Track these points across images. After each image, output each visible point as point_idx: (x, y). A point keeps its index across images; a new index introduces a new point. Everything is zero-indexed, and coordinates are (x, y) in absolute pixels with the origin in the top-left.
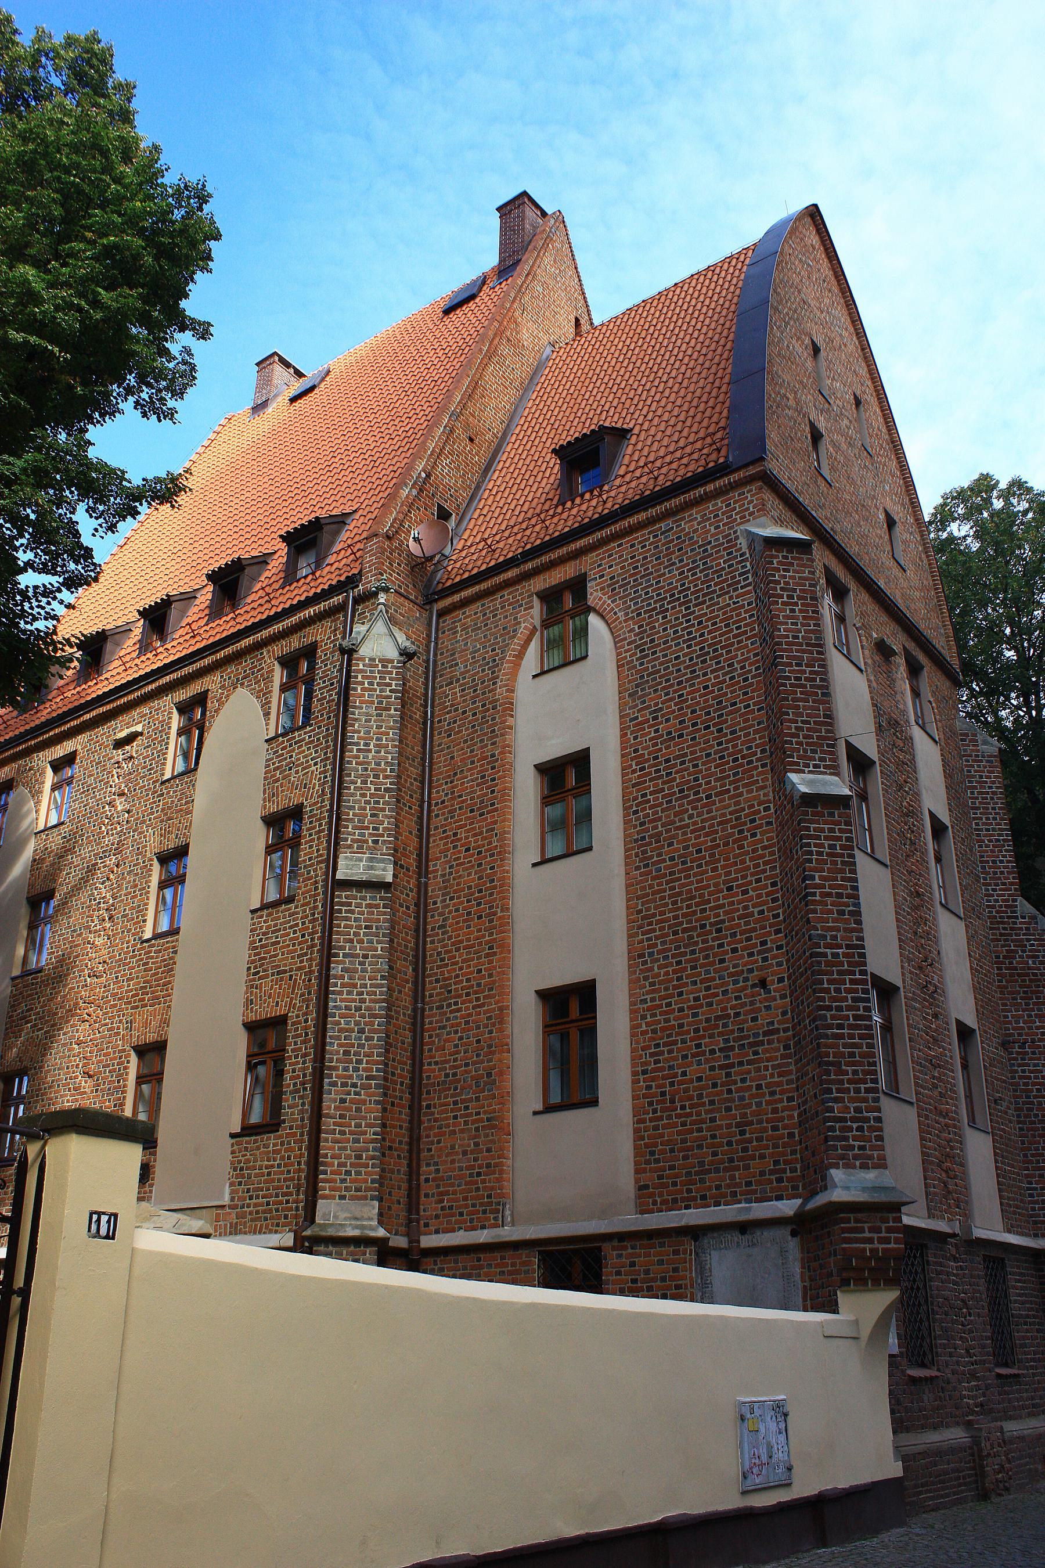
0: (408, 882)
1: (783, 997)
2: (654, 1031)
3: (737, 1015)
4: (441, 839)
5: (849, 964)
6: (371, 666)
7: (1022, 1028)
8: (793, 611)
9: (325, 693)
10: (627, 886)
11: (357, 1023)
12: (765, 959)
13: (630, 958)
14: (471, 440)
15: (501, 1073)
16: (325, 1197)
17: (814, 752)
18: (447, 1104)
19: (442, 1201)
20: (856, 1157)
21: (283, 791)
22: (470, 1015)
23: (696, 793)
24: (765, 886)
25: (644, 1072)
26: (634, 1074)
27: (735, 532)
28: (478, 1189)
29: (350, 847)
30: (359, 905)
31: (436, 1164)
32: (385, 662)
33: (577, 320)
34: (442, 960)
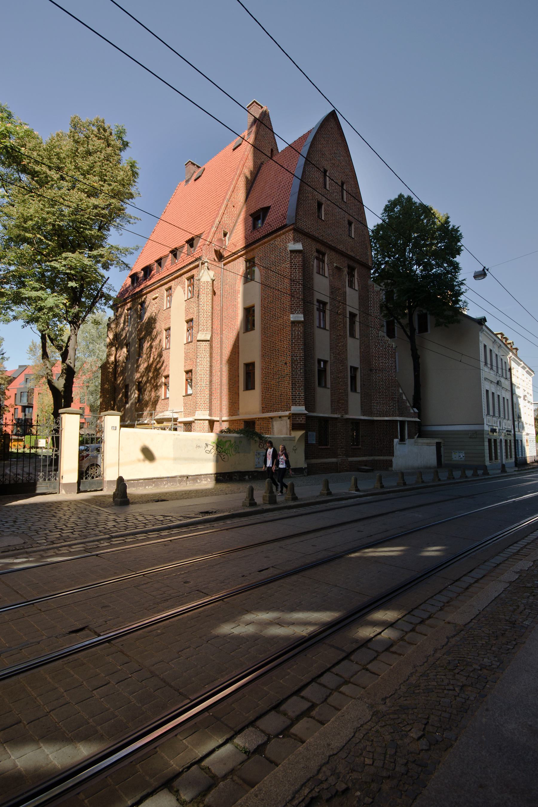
5: (300, 361)
14: (234, 207)
17: (298, 308)
20: (298, 403)
30: (202, 345)
32: (207, 282)
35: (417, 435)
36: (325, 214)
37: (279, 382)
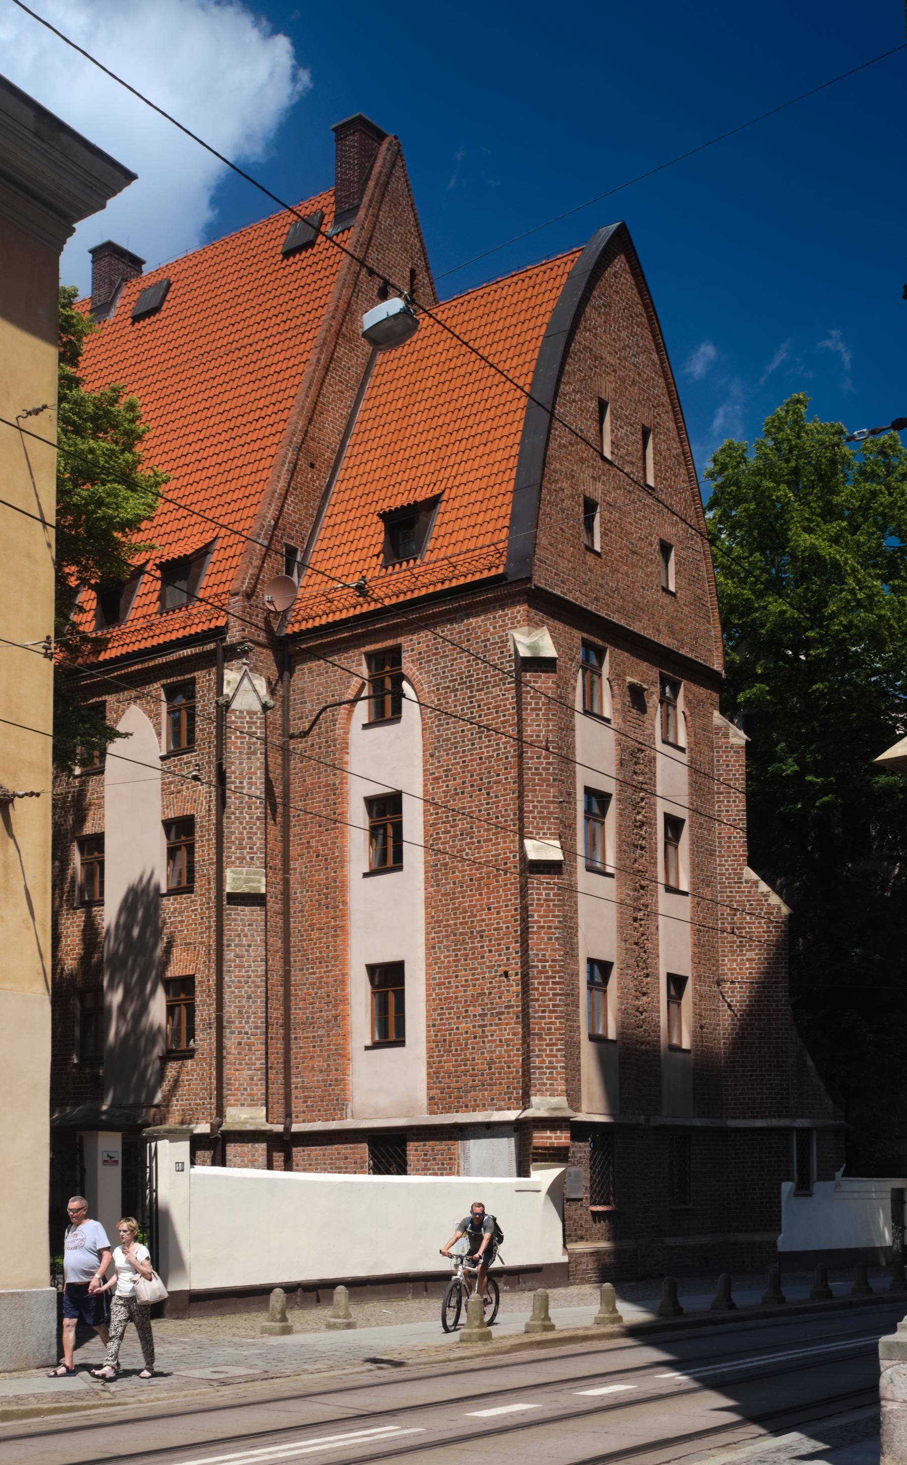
0: (276, 878)
1: (517, 985)
2: (440, 999)
3: (490, 993)
4: (298, 845)
6: (240, 717)
7: (735, 969)
8: (538, 715)
9: (204, 729)
10: (426, 898)
11: (246, 992)
12: (508, 959)
13: (427, 949)
14: (312, 466)
15: (344, 1018)
16: (232, 1105)
17: (544, 823)
18: (308, 1038)
19: (306, 1102)
21: (178, 802)
22: (322, 977)
23: (471, 838)
24: (510, 911)
25: (434, 1025)
26: (428, 1026)
27: (507, 635)
28: (330, 1095)
29: (233, 862)
31: (302, 1077)
32: (251, 713)
33: (413, 272)
34: (302, 936)
35: (842, 1169)
36: (603, 534)
37: (485, 1026)
